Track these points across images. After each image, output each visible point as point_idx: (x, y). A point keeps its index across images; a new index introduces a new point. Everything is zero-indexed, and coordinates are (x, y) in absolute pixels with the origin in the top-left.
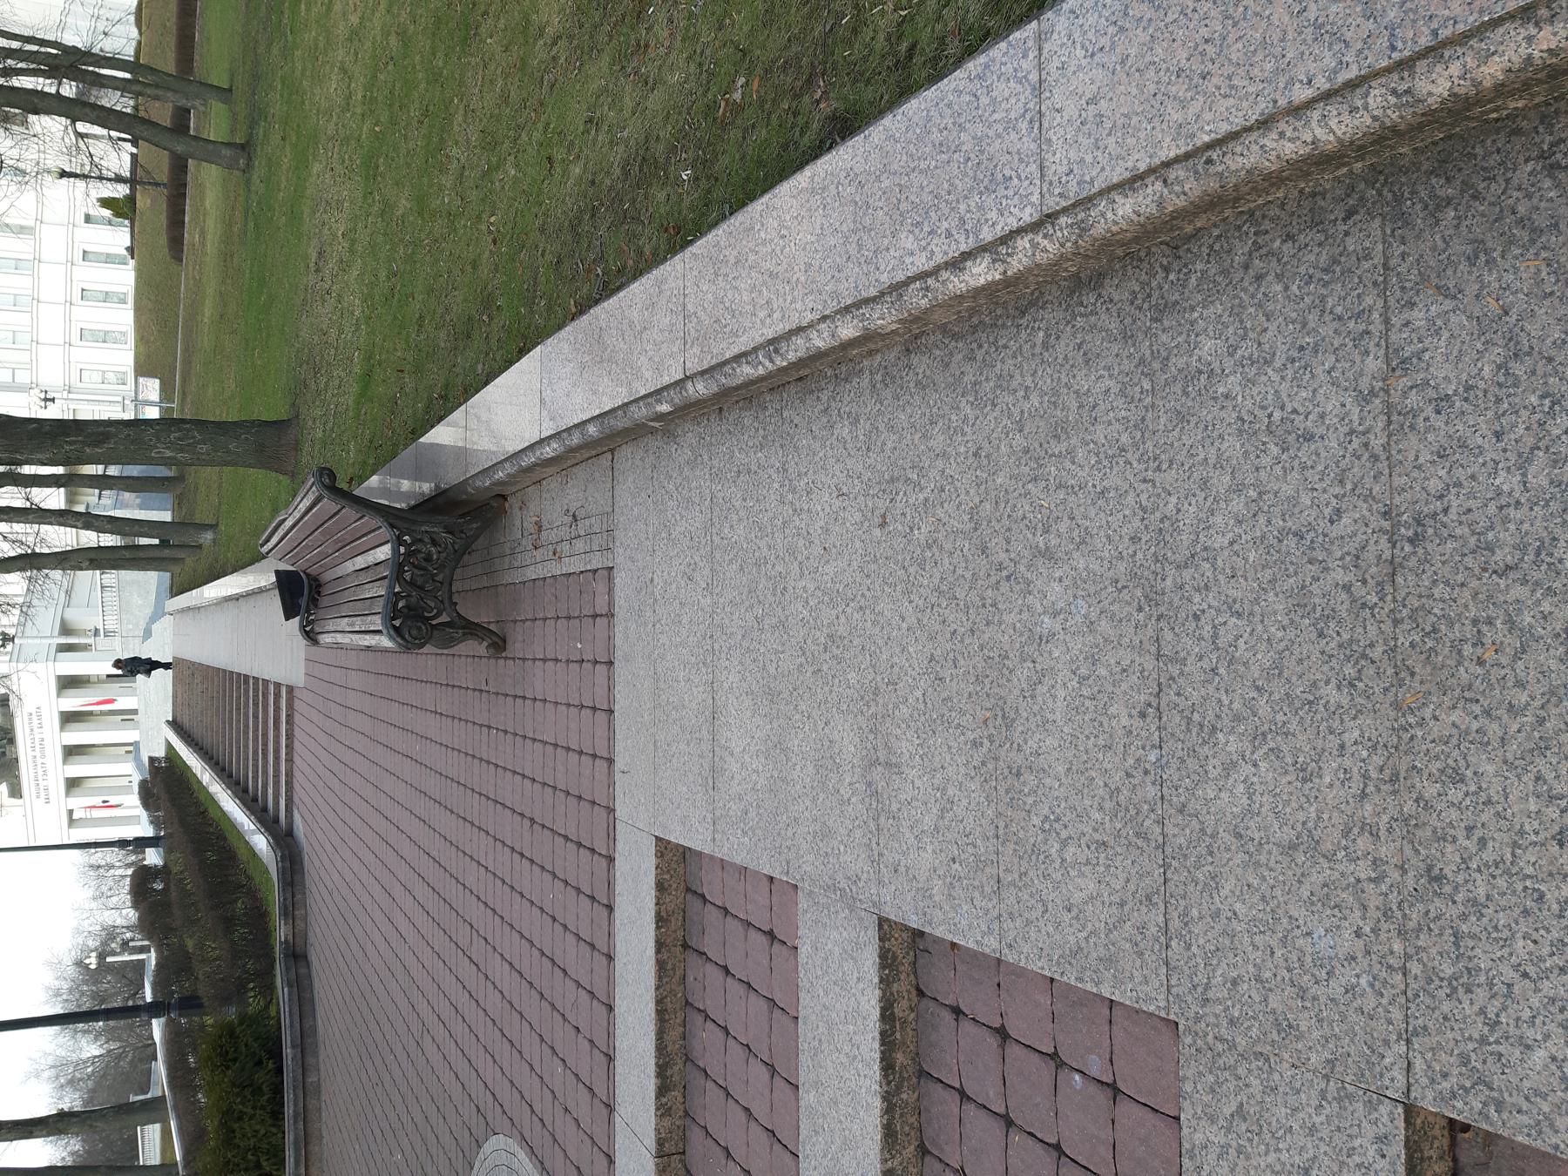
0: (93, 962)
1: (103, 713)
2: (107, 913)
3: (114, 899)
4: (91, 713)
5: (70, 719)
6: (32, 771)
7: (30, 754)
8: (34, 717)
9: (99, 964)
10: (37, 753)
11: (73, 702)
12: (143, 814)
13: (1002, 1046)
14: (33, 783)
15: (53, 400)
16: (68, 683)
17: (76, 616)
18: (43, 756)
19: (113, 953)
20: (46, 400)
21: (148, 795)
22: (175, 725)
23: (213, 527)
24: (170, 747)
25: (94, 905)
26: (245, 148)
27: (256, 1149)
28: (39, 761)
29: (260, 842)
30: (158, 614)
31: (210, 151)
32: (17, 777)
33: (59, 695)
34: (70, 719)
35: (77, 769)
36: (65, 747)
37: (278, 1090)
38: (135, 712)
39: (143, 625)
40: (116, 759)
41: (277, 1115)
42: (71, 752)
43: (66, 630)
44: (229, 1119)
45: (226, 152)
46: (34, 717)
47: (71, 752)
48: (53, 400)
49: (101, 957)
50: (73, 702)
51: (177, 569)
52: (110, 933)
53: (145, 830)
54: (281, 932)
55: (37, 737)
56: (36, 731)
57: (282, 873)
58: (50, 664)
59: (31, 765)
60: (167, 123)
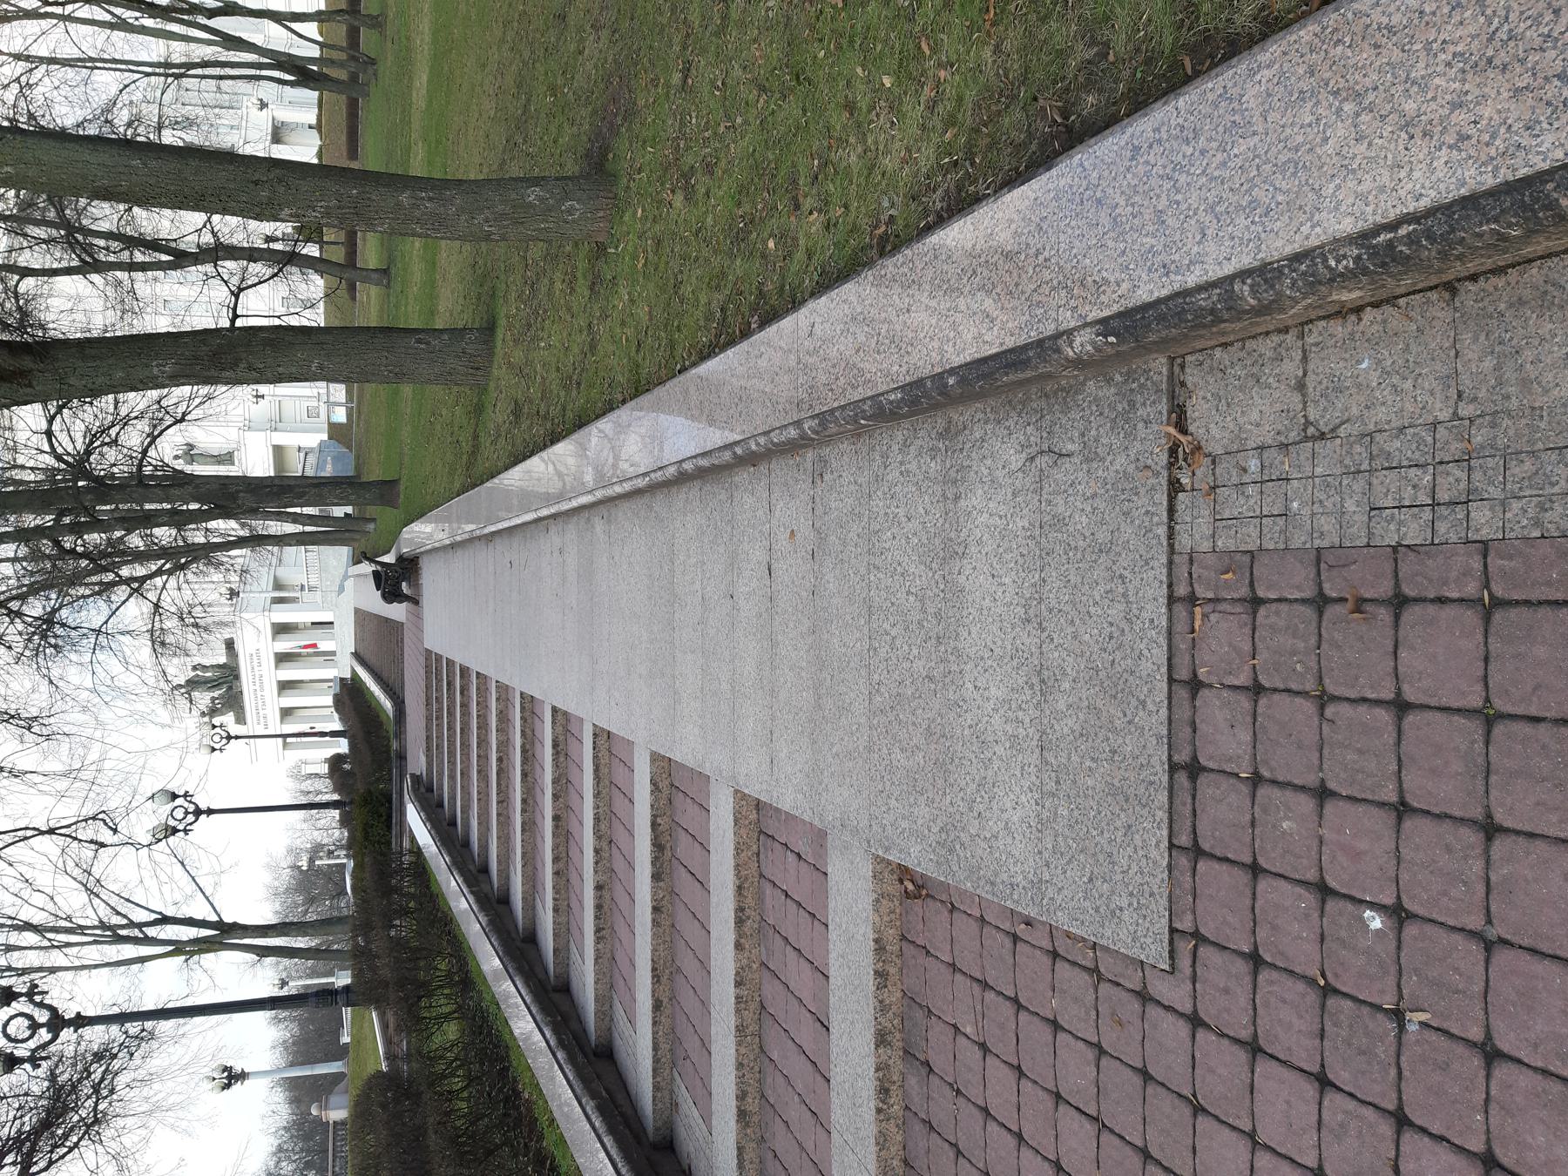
0: (304, 864)
1: (309, 655)
2: (316, 833)
3: (323, 822)
4: (299, 655)
5: (283, 658)
6: (253, 702)
7: (252, 687)
8: (255, 657)
9: (309, 866)
10: (257, 687)
11: (286, 645)
12: (336, 716)
13: (1400, 1107)
14: (254, 712)
15: (263, 397)
16: (281, 629)
17: (285, 574)
18: (262, 689)
19: (321, 858)
20: (257, 396)
21: (339, 703)
22: (357, 656)
23: (374, 520)
24: (353, 671)
25: (305, 826)
26: (385, 272)
27: (379, 842)
28: (259, 693)
29: (387, 704)
30: (346, 577)
31: (367, 275)
32: (242, 708)
33: (273, 640)
34: (283, 658)
35: (289, 701)
36: (279, 682)
37: (390, 817)
38: (333, 653)
39: (338, 582)
40: (320, 693)
41: (389, 827)
42: (285, 686)
43: (278, 586)
44: (366, 828)
45: (375, 276)
46: (255, 657)
47: (285, 686)
48: (263, 397)
49: (311, 861)
50: (286, 645)
51: (356, 545)
52: (316, 850)
53: (337, 726)
54: (395, 745)
55: (257, 673)
56: (256, 669)
57: (395, 716)
58: (266, 613)
59: (253, 697)
60: (342, 261)
